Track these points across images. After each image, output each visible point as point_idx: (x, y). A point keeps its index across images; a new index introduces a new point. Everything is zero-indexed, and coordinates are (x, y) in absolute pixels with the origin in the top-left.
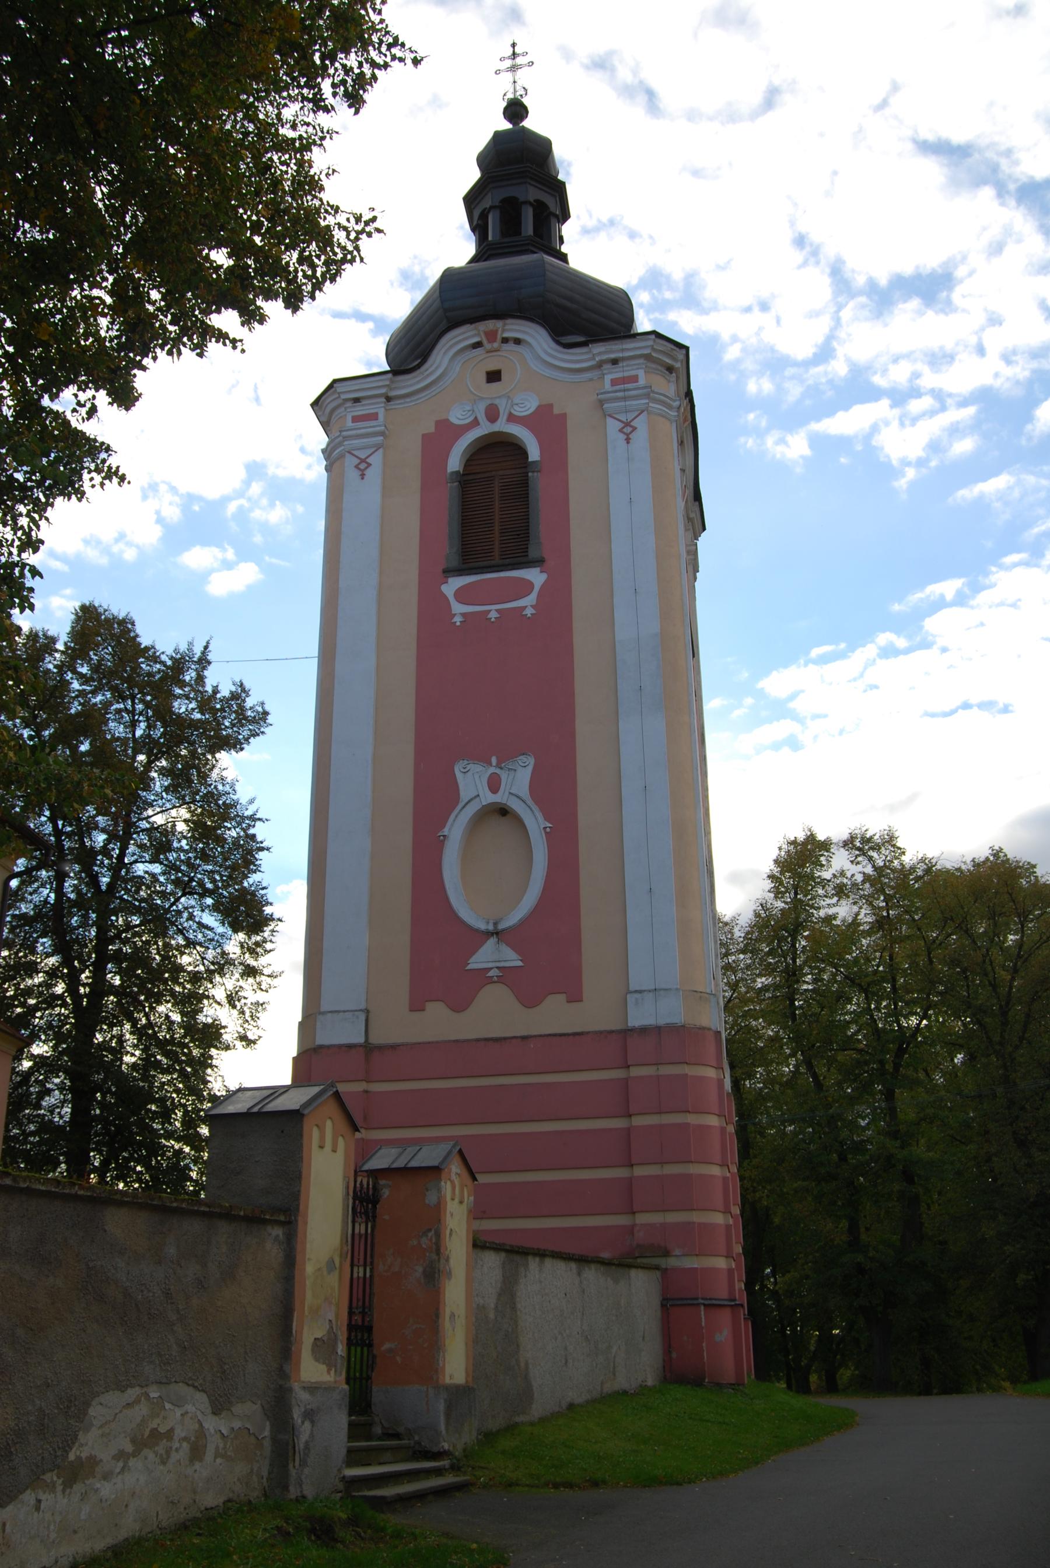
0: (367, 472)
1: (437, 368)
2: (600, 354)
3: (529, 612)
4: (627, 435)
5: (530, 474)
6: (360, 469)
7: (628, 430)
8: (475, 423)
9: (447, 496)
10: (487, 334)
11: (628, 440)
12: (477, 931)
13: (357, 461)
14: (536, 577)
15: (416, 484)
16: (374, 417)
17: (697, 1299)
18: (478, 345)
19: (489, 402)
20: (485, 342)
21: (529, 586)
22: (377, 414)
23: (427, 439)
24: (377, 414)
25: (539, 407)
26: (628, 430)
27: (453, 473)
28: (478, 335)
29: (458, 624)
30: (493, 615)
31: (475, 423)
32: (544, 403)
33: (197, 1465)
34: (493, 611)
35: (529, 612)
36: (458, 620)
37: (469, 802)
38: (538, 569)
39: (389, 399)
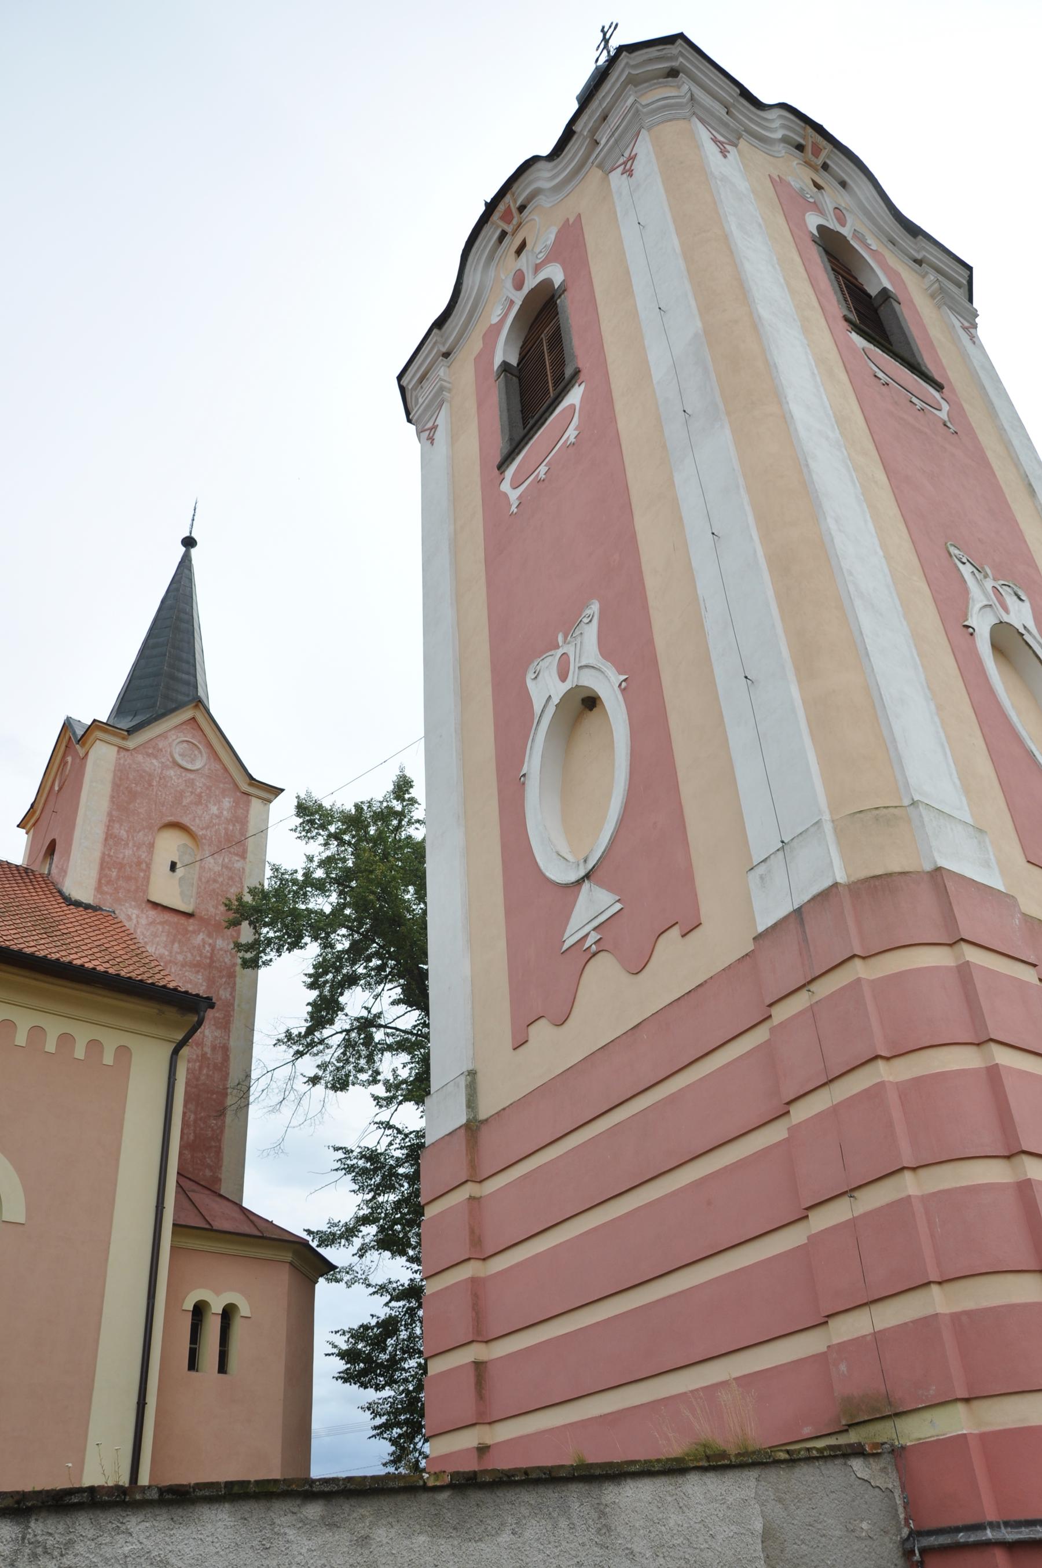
2: (586, 124)
12: (567, 886)
17: (979, 1527)
28: (498, 226)
33: (287, 1053)
37: (542, 711)
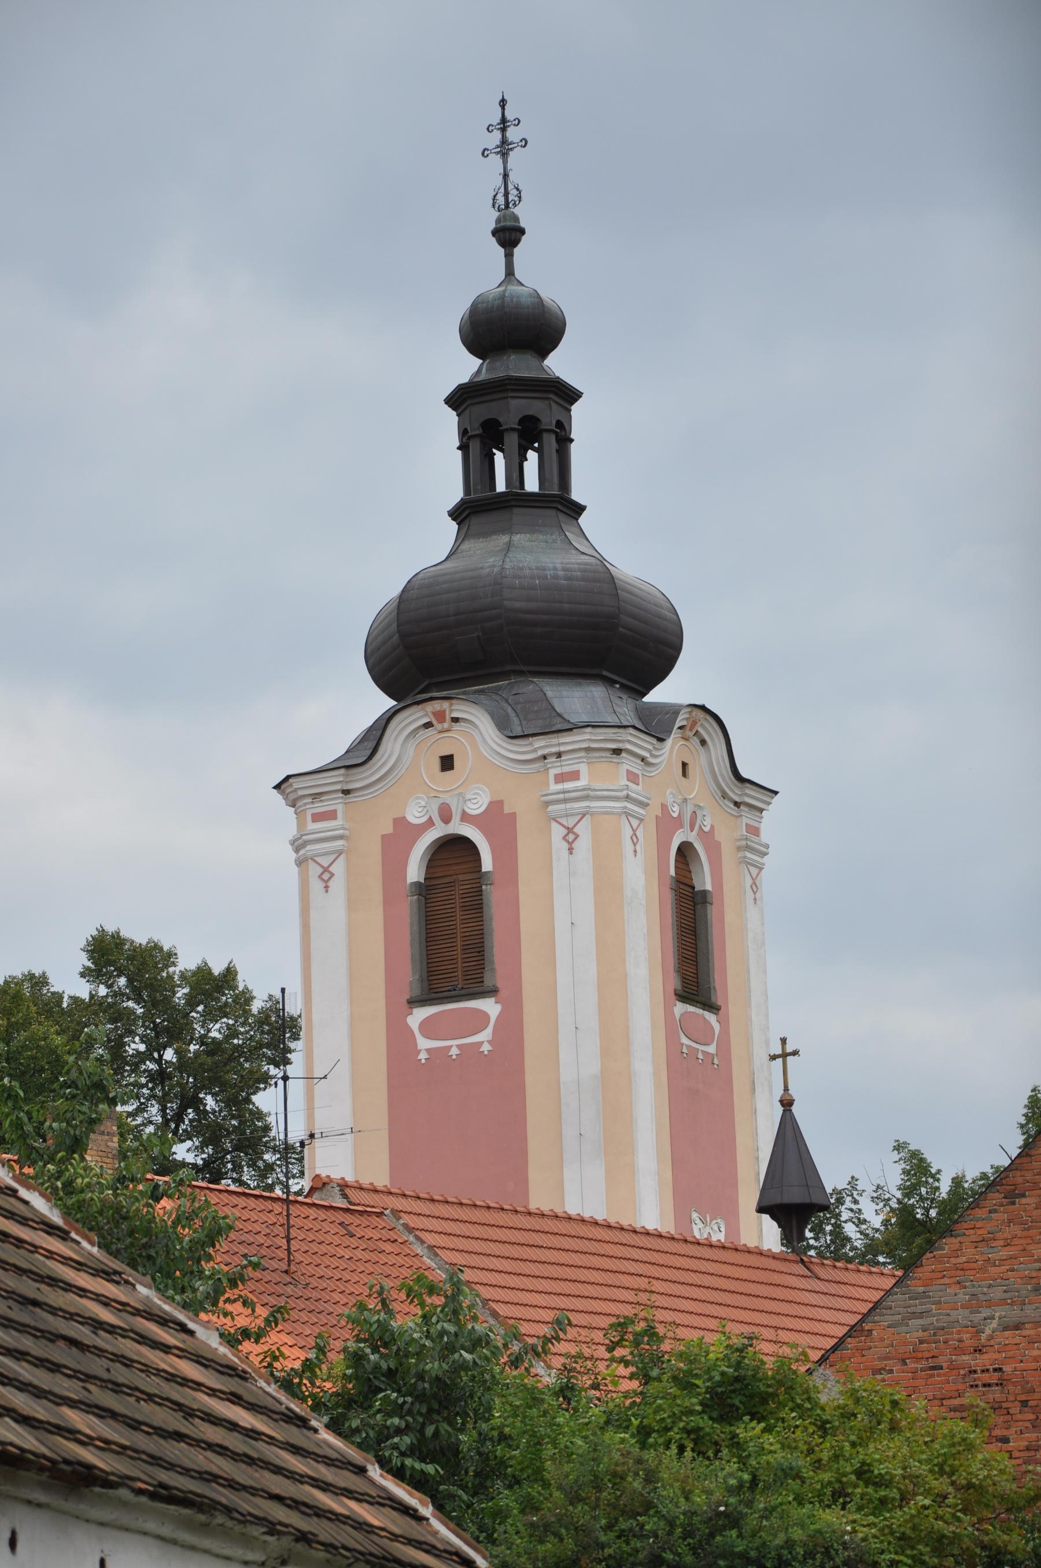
0: (330, 884)
1: (389, 757)
3: (486, 1048)
4: (570, 843)
5: (484, 887)
6: (323, 880)
7: (571, 835)
8: (430, 823)
9: (407, 909)
10: (435, 714)
11: (571, 850)
13: (321, 870)
14: (490, 1007)
15: (378, 896)
16: (332, 815)
18: (428, 725)
19: (441, 801)
20: (435, 722)
21: (481, 1019)
22: (335, 811)
23: (386, 840)
24: (335, 811)
25: (491, 803)
26: (571, 835)
27: (412, 884)
28: (426, 715)
29: (423, 1061)
30: (454, 1051)
31: (430, 823)
32: (495, 799)
34: (454, 1046)
35: (486, 1048)
36: (423, 1056)
38: (493, 1000)
39: (346, 792)
